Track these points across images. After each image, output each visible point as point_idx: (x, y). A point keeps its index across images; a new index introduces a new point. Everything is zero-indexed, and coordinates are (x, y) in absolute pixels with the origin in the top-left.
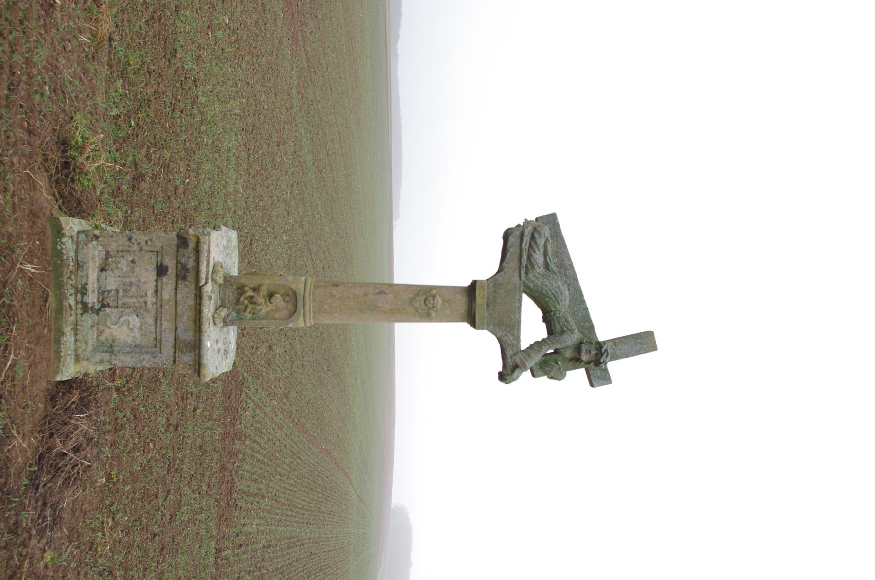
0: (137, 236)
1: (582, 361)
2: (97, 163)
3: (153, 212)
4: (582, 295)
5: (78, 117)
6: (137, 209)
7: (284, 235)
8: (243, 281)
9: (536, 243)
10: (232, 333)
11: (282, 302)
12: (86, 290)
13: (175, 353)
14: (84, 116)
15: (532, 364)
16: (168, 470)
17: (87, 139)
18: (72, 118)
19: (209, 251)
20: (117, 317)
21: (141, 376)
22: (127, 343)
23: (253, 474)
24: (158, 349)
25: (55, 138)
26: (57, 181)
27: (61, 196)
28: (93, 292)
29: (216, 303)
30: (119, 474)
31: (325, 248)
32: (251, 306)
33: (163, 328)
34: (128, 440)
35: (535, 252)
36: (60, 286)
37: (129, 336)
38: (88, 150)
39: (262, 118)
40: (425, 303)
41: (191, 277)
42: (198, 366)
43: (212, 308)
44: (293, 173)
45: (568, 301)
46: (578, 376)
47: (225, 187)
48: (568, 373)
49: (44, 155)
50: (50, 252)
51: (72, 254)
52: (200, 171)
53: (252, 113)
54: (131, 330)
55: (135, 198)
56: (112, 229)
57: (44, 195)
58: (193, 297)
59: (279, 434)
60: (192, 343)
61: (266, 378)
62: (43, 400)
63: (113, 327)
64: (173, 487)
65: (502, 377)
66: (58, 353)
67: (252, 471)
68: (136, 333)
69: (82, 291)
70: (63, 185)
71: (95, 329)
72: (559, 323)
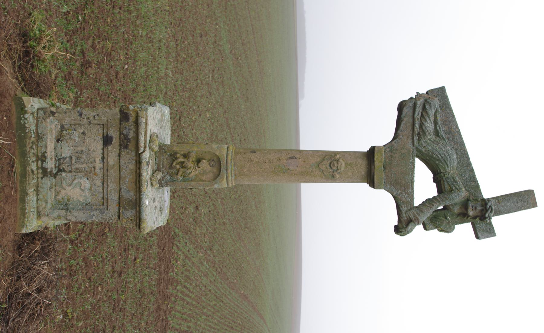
0: (87, 112)
1: (469, 216)
2: (52, 52)
3: (99, 93)
4: (468, 158)
5: (35, 13)
6: (85, 91)
7: (207, 113)
8: (176, 149)
9: (427, 113)
10: (166, 193)
11: (208, 166)
12: (46, 158)
13: (119, 210)
14: (40, 12)
15: (424, 219)
16: (114, 309)
17: (44, 31)
18: (30, 14)
19: (146, 124)
20: (71, 180)
21: (90, 231)
22: (80, 201)
23: (184, 314)
24: (105, 207)
25: (17, 31)
26: (19, 67)
27: (23, 79)
28: (51, 159)
29: (152, 167)
30: (73, 312)
31: (242, 124)
32: (182, 170)
33: (109, 189)
34: (81, 284)
35: (426, 121)
36: (24, 155)
37: (81, 195)
38: (45, 41)
39: (187, 13)
40: (330, 166)
41: (131, 145)
42: (139, 221)
43: (150, 172)
44: (214, 60)
45: (456, 163)
46: (465, 230)
47: (157, 72)
48: (457, 227)
49: (9, 45)
50: (15, 126)
51: (33, 128)
52: (137, 59)
53: (179, 8)
54: (83, 190)
55: (83, 82)
56: (66, 106)
57: (10, 79)
58: (134, 162)
59: (204, 281)
60: (133, 201)
61: (194, 234)
62: (12, 249)
63: (67, 188)
64: (118, 324)
65: (398, 230)
66: (23, 210)
67: (182, 311)
68: (87, 193)
69: (42, 158)
70: (25, 70)
71: (53, 190)
72: (448, 182)
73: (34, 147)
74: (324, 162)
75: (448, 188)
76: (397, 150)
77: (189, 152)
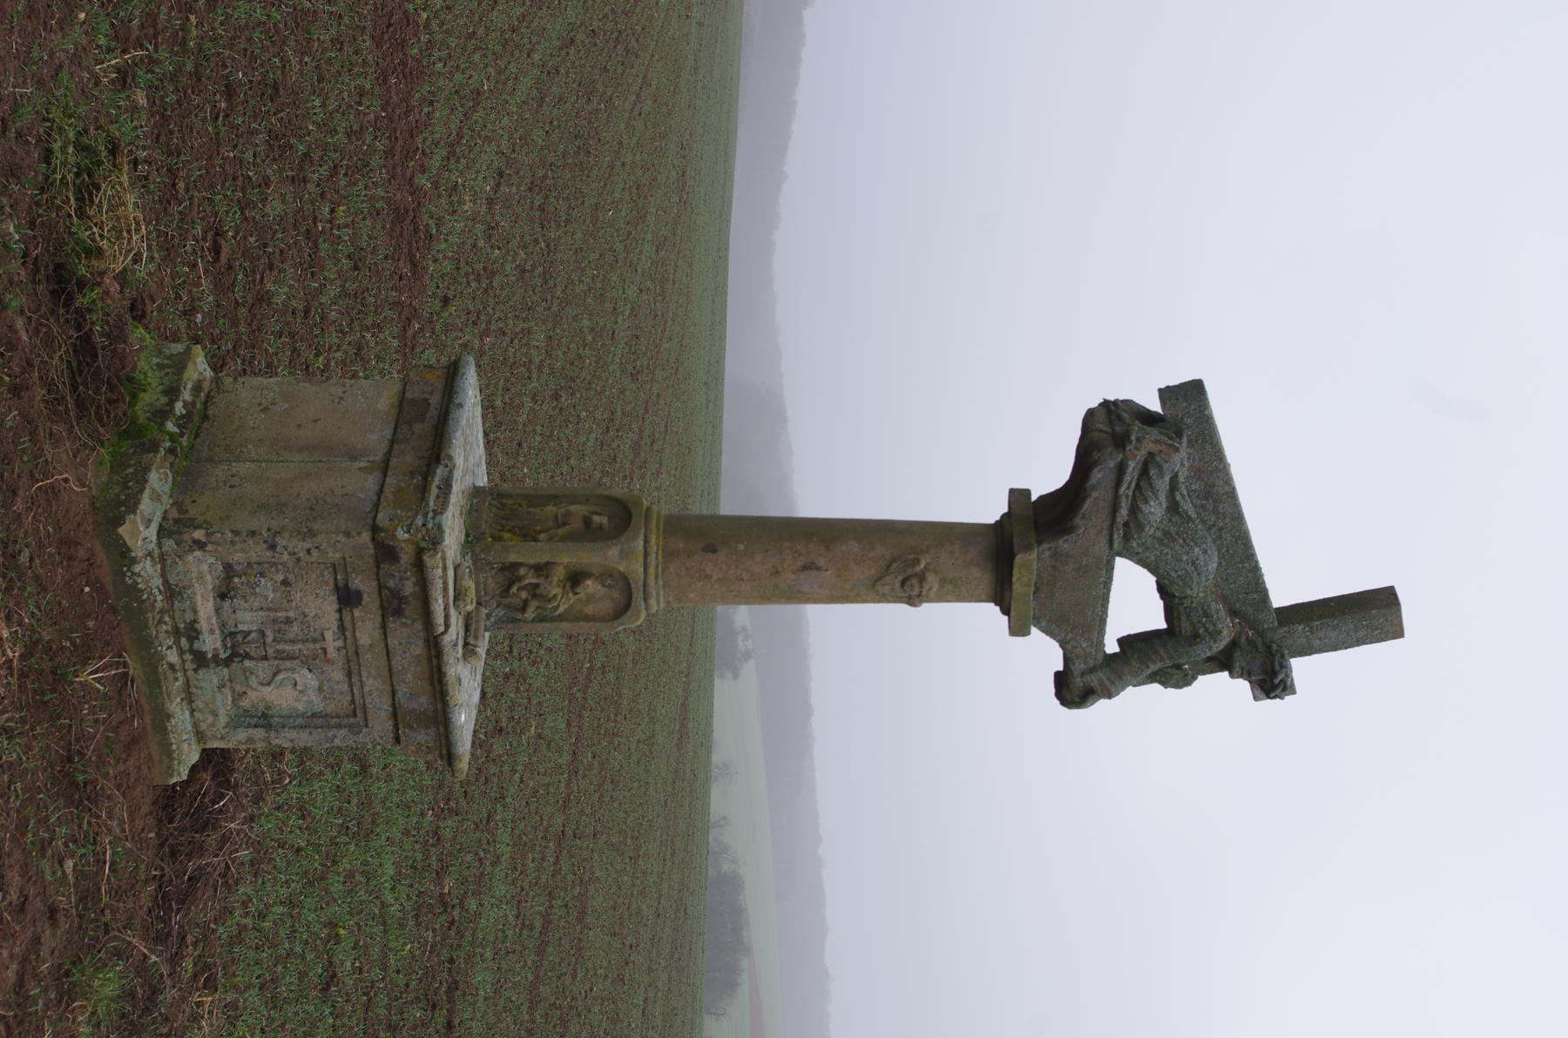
12: (198, 633)
13: (396, 727)
33: (366, 689)
40: (899, 560)
41: (411, 610)
58: (421, 643)
69: (192, 632)
71: (227, 691)
72: (1188, 616)
73: (167, 619)
74: (888, 579)
75: (1189, 629)
76: (1068, 556)
77: (547, 564)
